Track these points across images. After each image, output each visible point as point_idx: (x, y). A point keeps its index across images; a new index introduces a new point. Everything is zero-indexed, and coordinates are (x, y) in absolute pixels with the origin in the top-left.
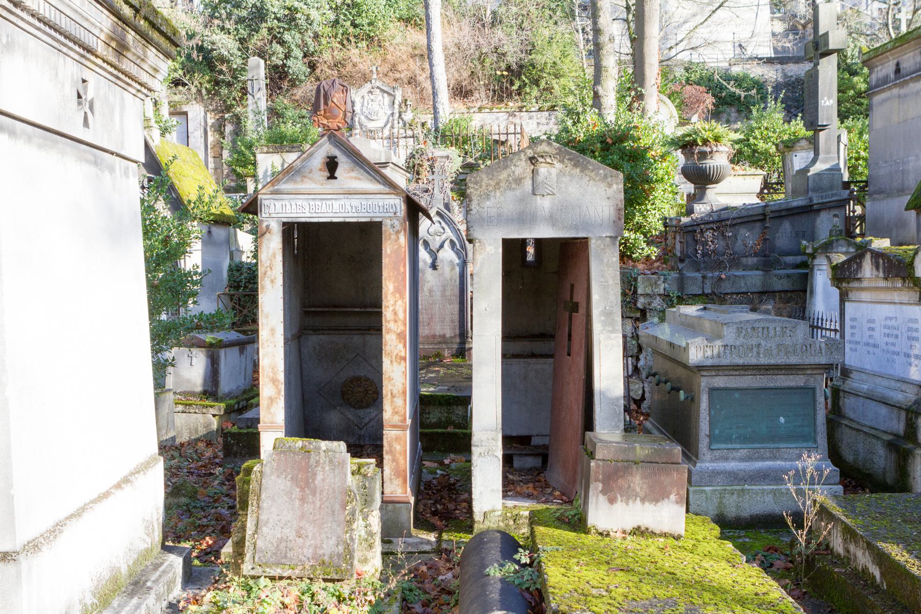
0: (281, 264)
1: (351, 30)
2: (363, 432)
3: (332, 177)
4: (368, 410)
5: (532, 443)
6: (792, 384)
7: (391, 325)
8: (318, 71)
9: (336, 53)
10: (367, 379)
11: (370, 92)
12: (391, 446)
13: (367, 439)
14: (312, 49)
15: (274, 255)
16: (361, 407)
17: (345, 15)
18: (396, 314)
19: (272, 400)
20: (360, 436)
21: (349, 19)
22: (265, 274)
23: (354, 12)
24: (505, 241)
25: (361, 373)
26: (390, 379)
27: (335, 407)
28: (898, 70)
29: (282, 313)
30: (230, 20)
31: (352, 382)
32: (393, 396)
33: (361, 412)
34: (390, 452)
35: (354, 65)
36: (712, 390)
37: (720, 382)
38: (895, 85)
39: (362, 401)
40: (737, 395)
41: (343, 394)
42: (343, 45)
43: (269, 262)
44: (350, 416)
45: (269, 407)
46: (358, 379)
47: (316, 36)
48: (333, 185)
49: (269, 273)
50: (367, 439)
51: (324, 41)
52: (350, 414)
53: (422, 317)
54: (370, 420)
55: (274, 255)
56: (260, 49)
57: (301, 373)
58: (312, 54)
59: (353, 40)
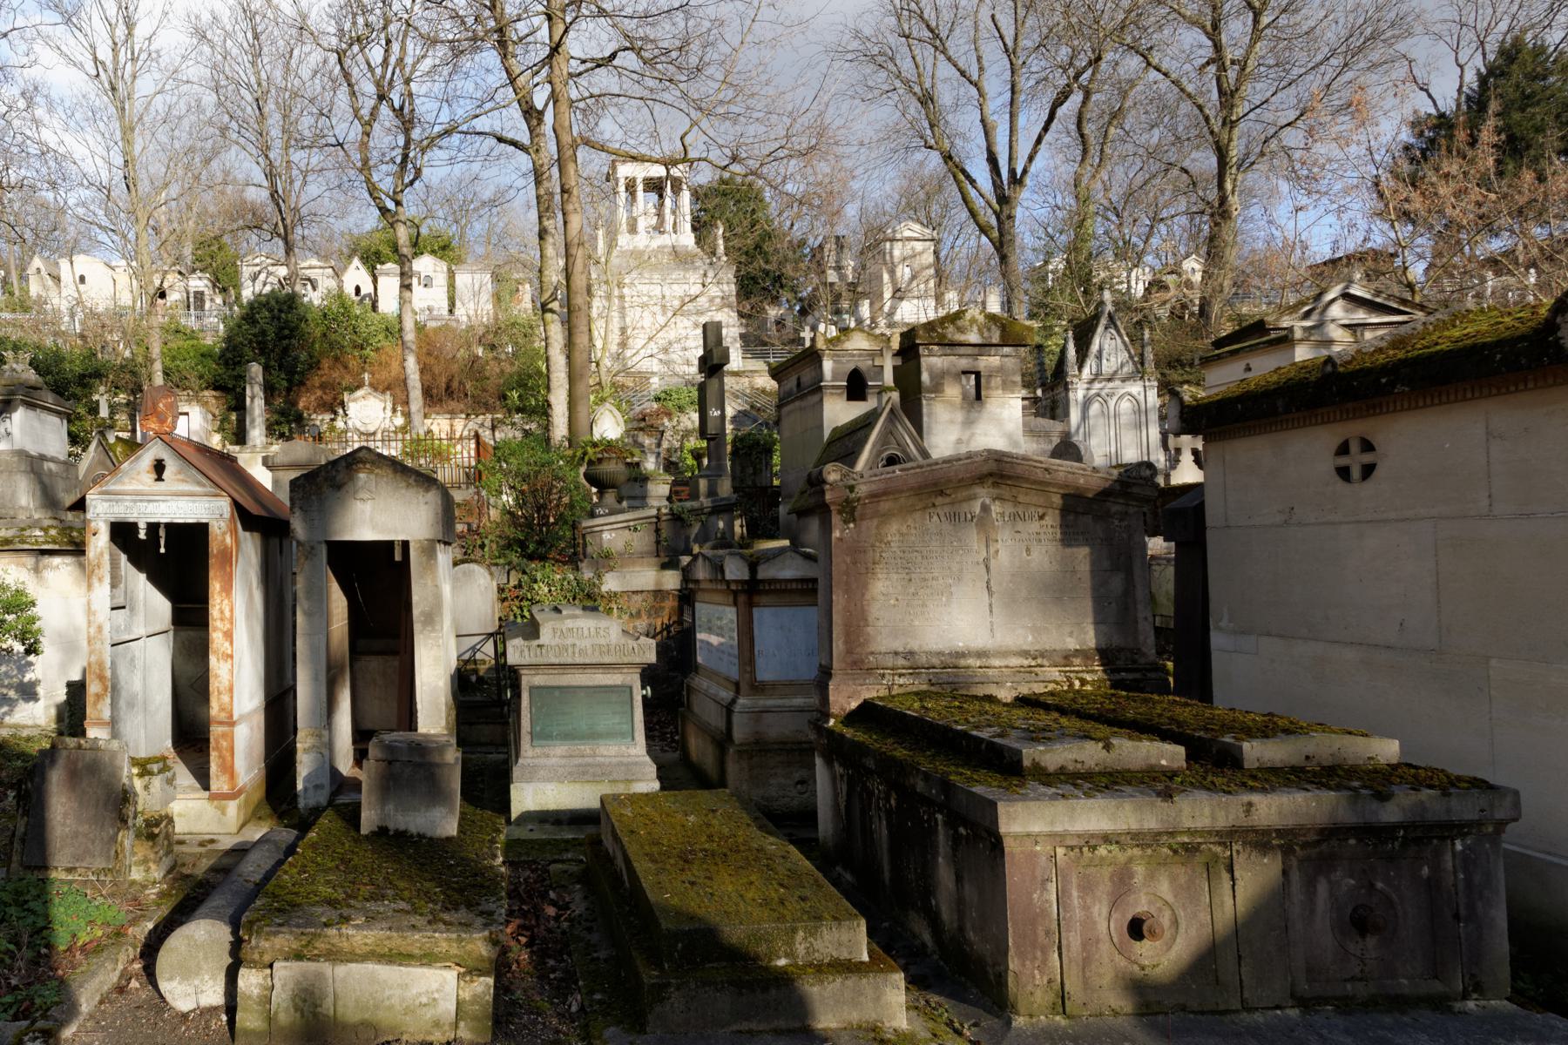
3: (159, 479)
5: (516, 809)
6: (610, 682)
7: (218, 624)
12: (217, 742)
15: (102, 554)
18: (222, 612)
19: (98, 697)
24: (206, 525)
26: (217, 676)
28: (799, 385)
29: (569, 807)
32: (220, 693)
34: (217, 749)
36: (532, 689)
37: (540, 680)
38: (797, 398)
40: (557, 693)
45: (95, 704)
48: (161, 486)
56: (1544, 130)
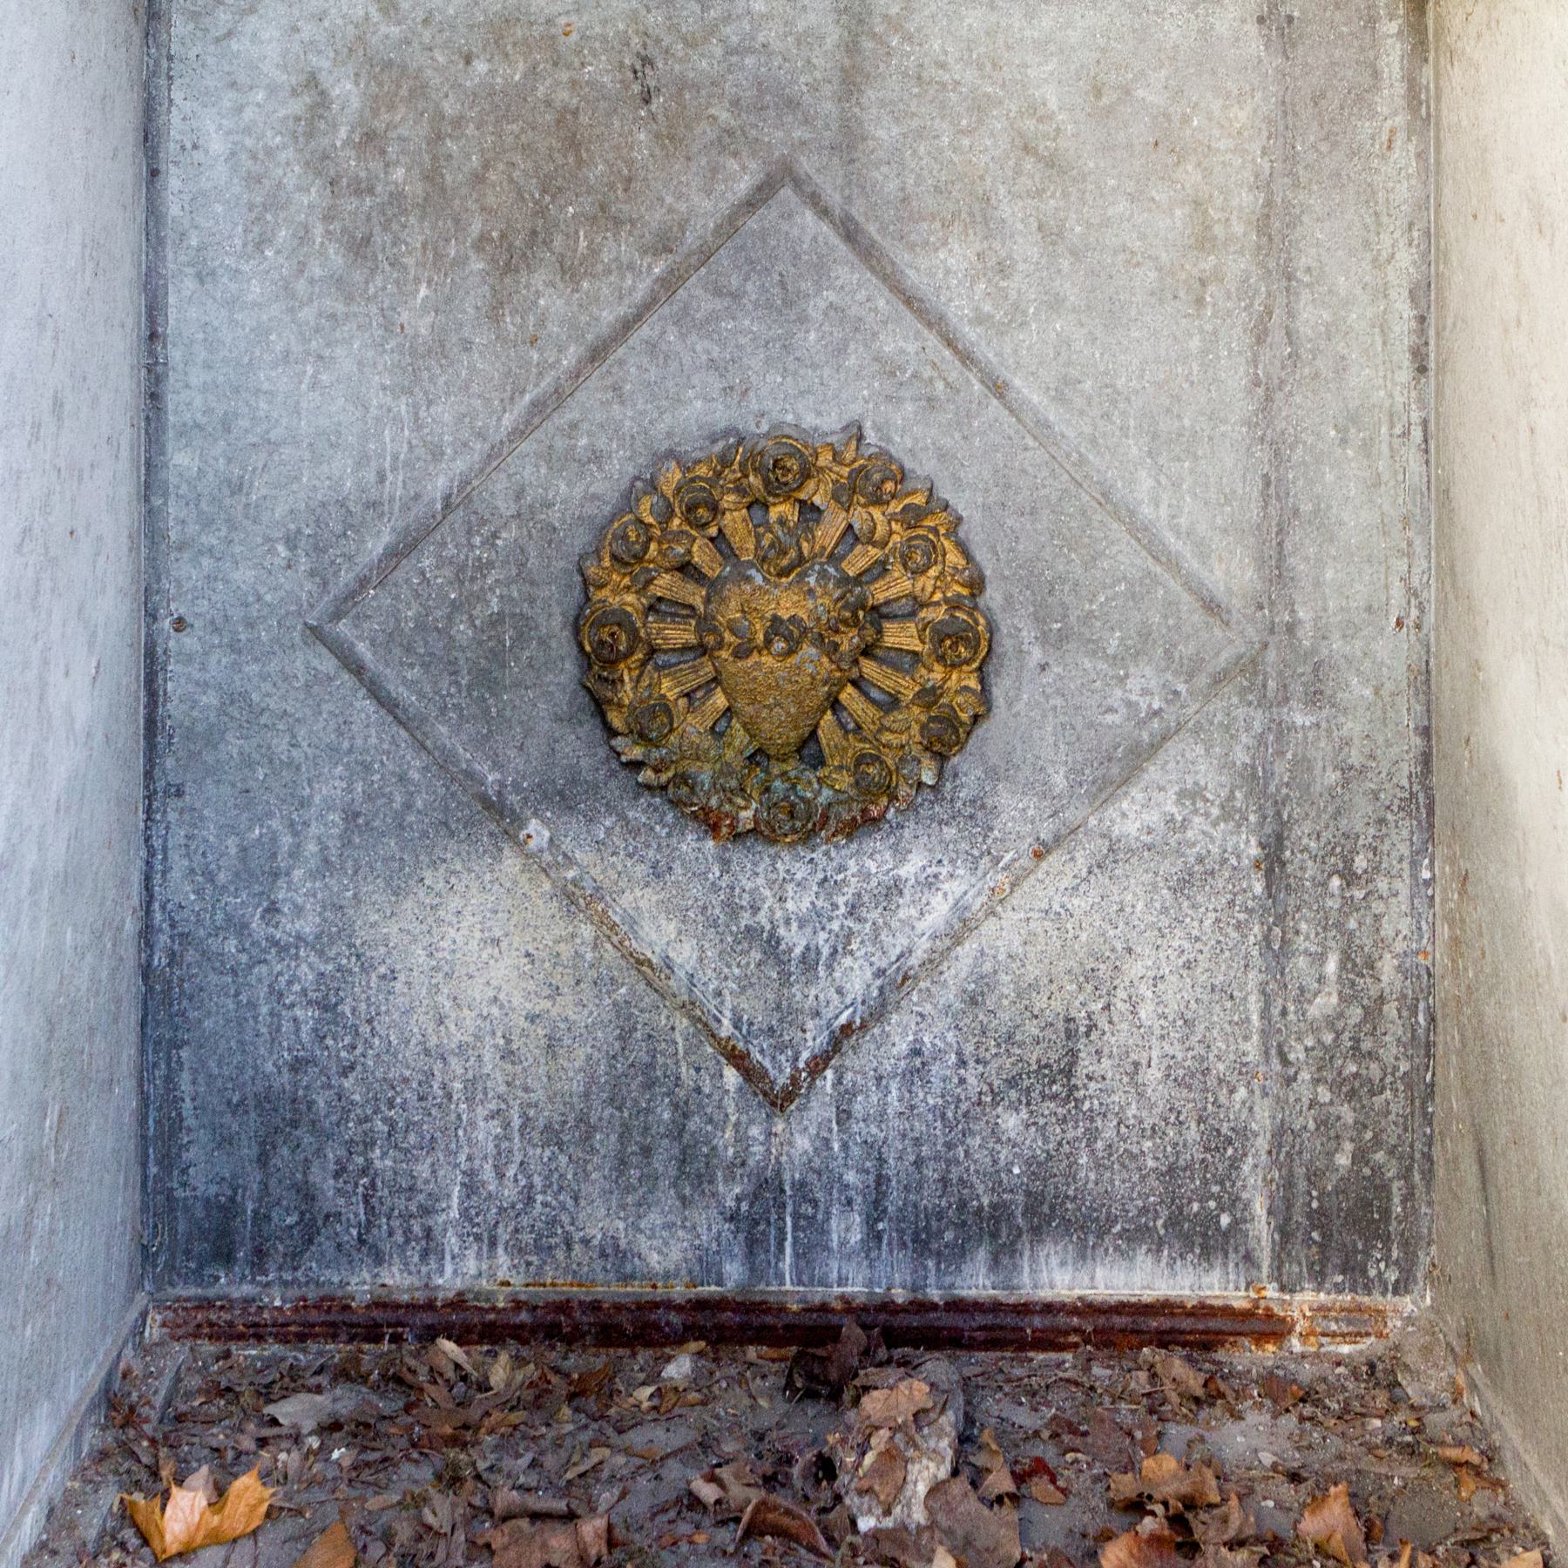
2: (797, 1140)
4: (869, 861)
10: (875, 478)
13: (846, 1228)
16: (799, 826)
20: (767, 1187)
25: (811, 401)
27: (499, 816)
30: (1127, 437)
31: (699, 507)
33: (790, 888)
39: (808, 749)
41: (602, 651)
44: (661, 935)
46: (774, 470)
50: (846, 1228)
52: (671, 904)
53: (183, 402)
54: (895, 984)
57: (154, 397)
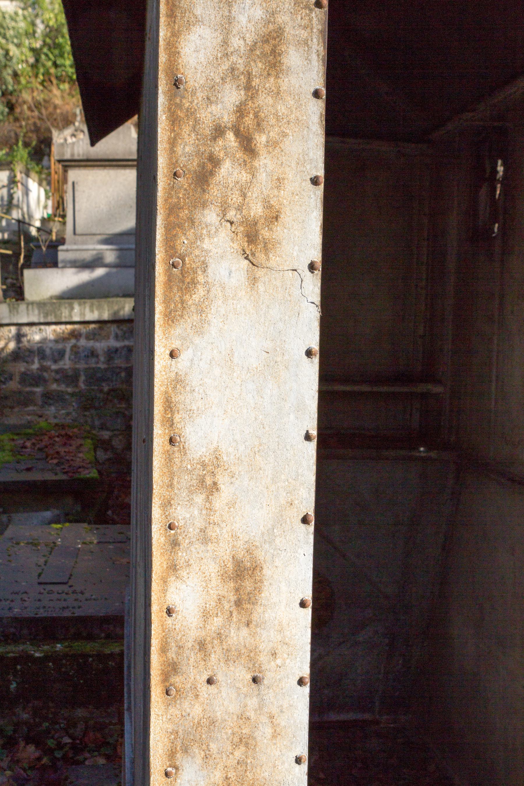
0: (315, 112)
1: (53, 71)
8: (18, 110)
9: (35, 94)
11: (73, 135)
14: (10, 88)
15: (270, 47)
17: (47, 55)
21: (50, 59)
22: (203, 177)
23: (56, 52)
35: (55, 107)
42: (44, 86)
43: (231, 96)
47: (15, 75)
49: (229, 172)
51: (23, 81)
55: (270, 47)
58: (11, 93)
59: (55, 81)
